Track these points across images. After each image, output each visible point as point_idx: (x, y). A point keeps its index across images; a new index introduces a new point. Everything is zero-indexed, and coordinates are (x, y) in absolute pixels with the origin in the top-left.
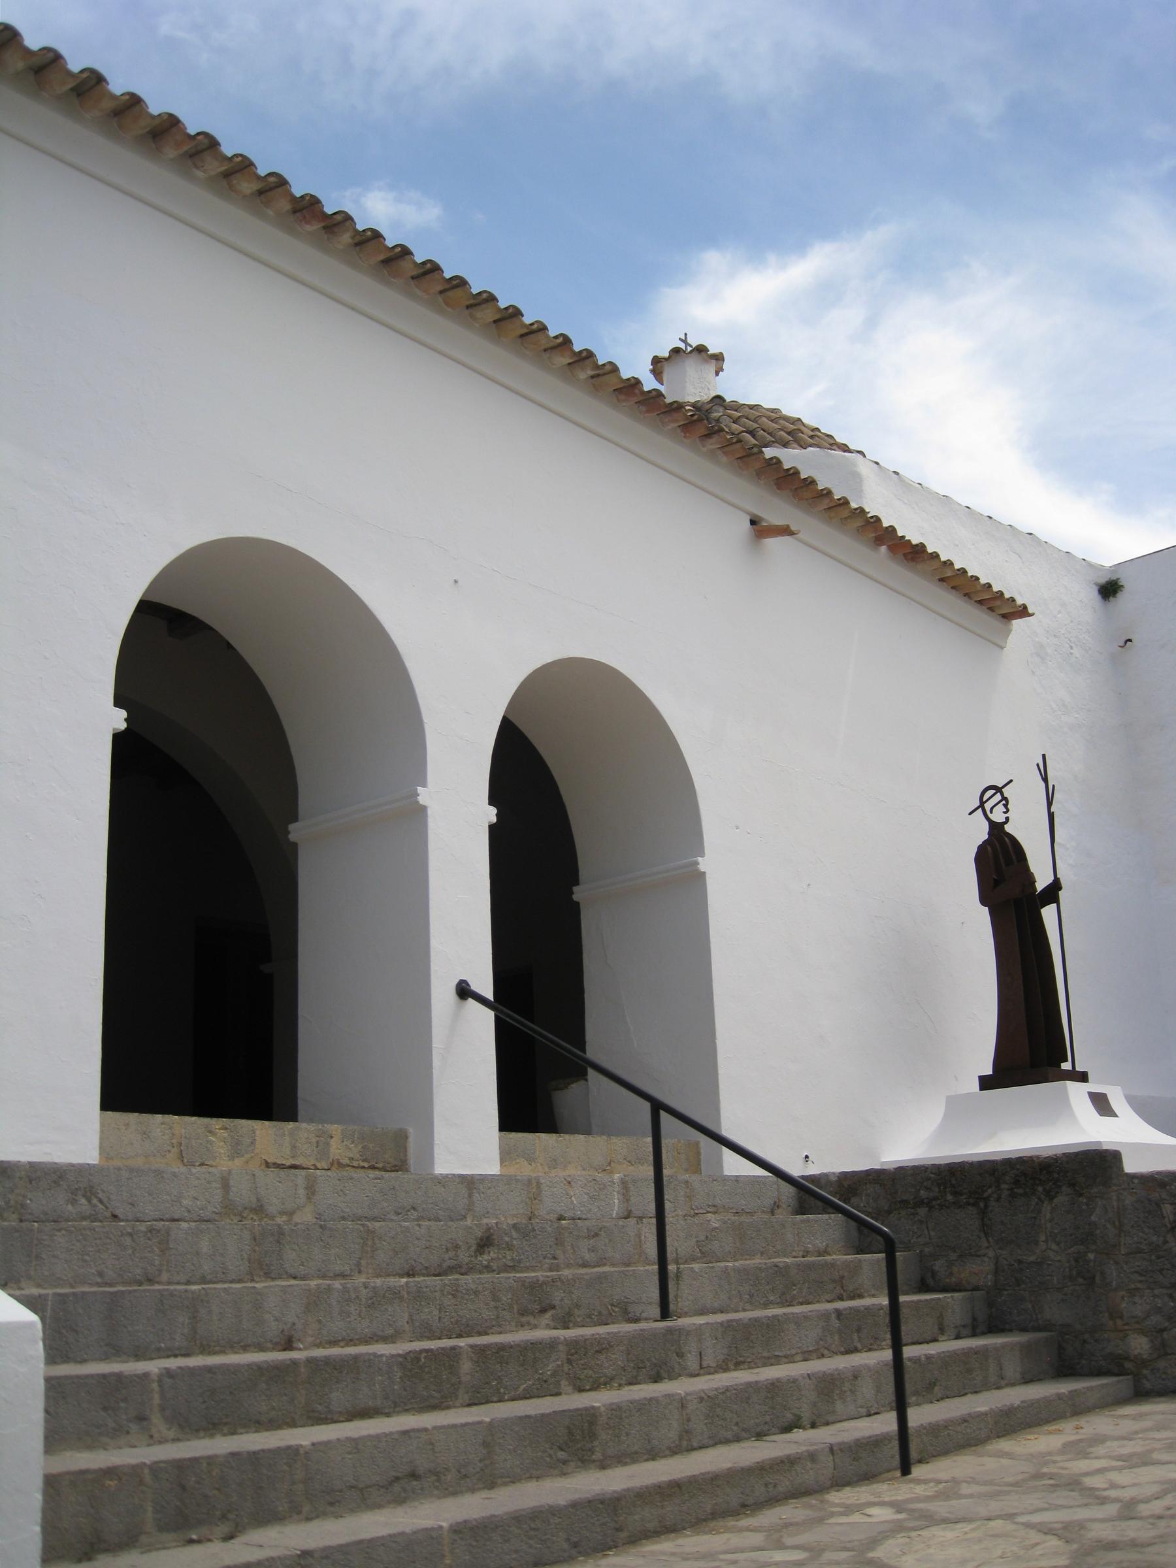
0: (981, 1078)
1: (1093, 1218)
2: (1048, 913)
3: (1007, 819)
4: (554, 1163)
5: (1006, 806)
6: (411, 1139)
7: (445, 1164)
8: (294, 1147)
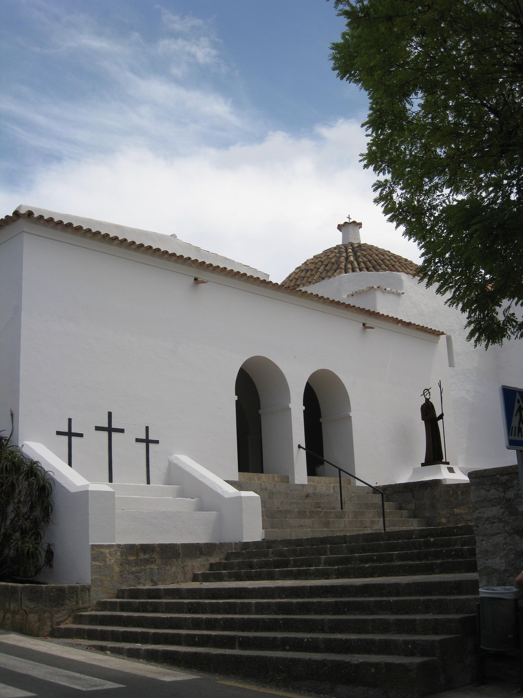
0: (422, 464)
1: (435, 494)
2: (440, 422)
3: (430, 398)
4: (318, 483)
5: (430, 394)
6: (290, 477)
7: (297, 482)
8: (268, 479)
